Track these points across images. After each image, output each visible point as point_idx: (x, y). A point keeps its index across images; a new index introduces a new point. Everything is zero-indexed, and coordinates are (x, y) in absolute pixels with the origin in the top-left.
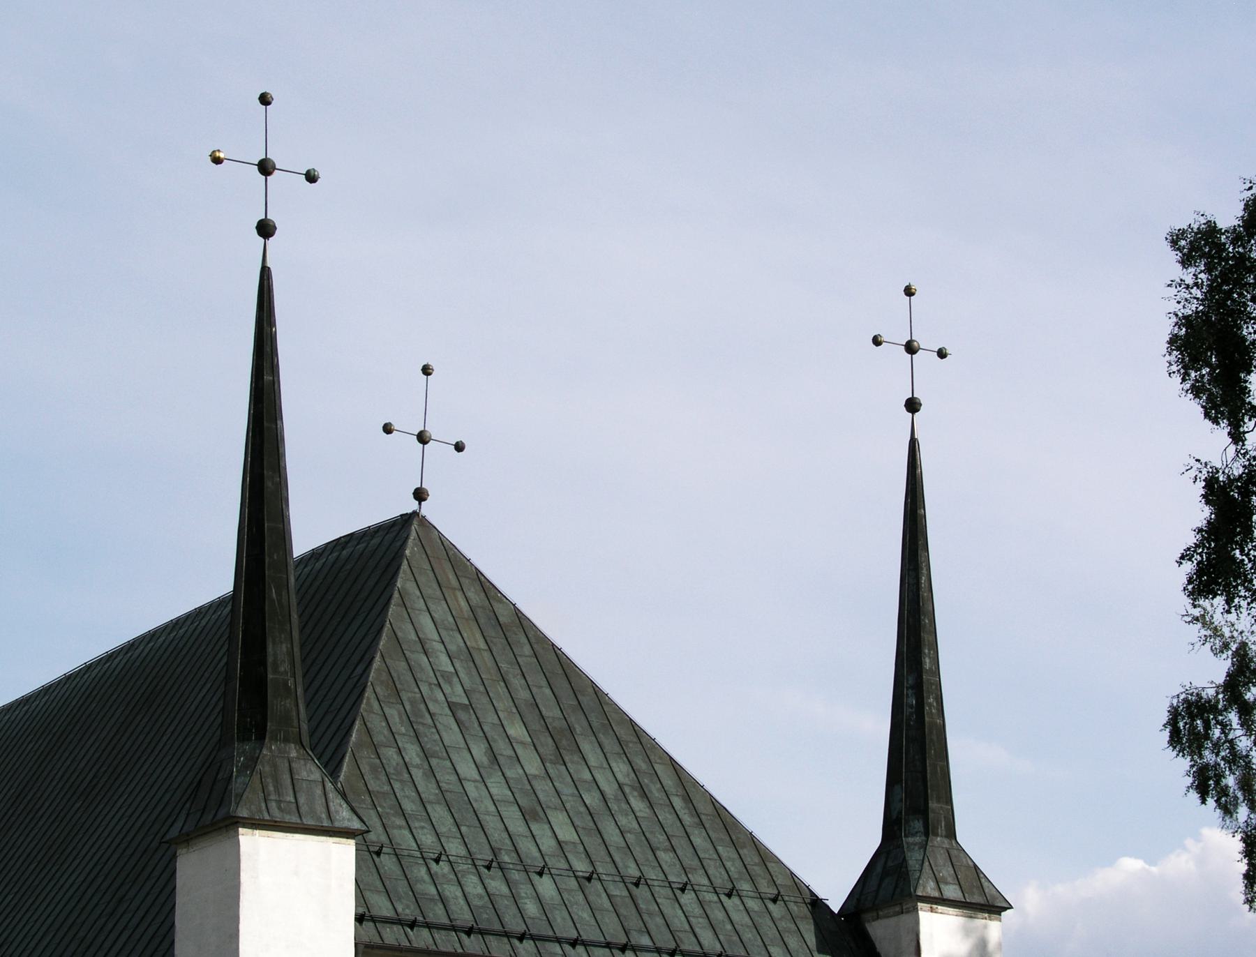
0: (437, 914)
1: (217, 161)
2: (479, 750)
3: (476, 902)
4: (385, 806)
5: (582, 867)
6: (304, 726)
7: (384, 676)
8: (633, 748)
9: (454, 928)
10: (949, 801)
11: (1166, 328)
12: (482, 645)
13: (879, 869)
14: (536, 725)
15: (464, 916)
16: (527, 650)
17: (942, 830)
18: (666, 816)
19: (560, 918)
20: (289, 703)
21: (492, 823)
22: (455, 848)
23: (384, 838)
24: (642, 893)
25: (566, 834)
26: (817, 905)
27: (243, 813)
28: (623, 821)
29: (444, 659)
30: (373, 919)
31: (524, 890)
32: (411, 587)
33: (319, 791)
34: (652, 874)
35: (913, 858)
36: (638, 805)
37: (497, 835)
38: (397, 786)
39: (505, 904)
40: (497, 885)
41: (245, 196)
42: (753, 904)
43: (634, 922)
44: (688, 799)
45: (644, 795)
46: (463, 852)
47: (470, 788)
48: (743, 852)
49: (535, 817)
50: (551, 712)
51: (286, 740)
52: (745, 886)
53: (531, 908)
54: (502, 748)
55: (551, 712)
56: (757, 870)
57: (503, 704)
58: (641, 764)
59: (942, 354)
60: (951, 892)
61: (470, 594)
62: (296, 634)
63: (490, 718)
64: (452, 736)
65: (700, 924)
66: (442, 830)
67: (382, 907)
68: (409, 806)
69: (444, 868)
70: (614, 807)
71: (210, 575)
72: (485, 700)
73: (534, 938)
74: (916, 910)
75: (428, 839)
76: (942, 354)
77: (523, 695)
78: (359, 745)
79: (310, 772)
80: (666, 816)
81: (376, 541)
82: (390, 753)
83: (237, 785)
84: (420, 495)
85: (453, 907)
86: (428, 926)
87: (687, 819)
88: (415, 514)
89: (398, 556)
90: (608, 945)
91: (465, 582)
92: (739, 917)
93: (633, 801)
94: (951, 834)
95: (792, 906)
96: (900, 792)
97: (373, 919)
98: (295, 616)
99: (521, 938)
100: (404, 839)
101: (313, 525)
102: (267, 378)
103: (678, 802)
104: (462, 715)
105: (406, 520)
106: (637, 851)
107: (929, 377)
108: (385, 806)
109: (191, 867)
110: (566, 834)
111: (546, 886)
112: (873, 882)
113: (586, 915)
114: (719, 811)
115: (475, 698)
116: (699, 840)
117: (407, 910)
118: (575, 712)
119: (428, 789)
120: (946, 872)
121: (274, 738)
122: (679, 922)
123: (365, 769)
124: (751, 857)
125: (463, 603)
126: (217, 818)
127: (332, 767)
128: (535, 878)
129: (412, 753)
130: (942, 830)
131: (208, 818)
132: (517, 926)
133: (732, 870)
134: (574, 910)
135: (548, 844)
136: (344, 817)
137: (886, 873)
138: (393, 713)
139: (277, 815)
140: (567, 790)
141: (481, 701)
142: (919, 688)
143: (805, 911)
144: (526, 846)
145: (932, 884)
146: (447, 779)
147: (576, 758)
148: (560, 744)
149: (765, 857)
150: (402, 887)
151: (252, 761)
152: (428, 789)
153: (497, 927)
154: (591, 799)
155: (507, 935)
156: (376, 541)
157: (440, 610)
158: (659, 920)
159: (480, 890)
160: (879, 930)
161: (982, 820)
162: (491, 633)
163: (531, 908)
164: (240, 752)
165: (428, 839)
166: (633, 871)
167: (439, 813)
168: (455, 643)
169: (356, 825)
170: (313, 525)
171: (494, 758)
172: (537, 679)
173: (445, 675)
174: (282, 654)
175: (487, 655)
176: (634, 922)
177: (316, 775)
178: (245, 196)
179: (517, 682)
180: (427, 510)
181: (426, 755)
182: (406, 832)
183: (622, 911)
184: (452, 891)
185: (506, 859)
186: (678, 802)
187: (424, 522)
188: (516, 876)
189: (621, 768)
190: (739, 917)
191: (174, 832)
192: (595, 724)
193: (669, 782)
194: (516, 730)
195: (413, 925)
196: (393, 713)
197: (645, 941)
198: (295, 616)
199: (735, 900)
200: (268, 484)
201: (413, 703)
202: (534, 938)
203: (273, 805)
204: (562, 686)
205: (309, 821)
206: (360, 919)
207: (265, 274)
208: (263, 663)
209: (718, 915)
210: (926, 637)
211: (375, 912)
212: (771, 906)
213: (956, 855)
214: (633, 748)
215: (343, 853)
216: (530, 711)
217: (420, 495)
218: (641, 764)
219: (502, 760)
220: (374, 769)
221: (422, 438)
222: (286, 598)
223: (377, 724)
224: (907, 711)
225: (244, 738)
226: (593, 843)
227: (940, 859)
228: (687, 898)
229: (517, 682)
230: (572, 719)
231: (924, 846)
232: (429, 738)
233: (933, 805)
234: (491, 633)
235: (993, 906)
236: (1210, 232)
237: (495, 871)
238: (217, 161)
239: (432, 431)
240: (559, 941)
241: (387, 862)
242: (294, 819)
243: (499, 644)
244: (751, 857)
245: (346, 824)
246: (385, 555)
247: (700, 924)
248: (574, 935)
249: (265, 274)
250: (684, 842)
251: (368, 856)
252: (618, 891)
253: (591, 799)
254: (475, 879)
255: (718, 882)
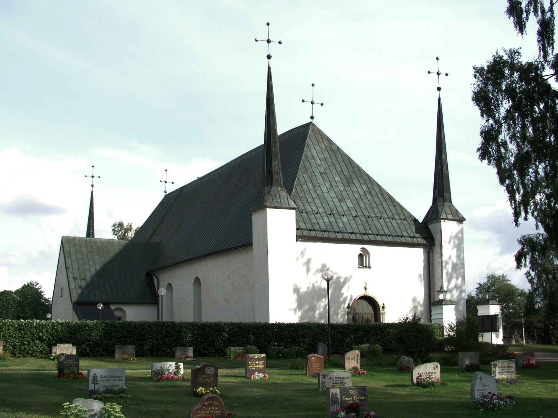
0: (317, 227)
1: (257, 41)
2: (328, 184)
3: (327, 224)
4: (304, 200)
5: (354, 213)
6: (282, 182)
7: (303, 166)
8: (368, 182)
9: (321, 231)
10: (450, 193)
11: (471, 95)
12: (329, 156)
13: (431, 211)
14: (342, 177)
15: (324, 228)
16: (340, 157)
17: (448, 200)
18: (376, 199)
19: (348, 227)
20: (278, 176)
21: (331, 203)
22: (321, 210)
23: (303, 208)
24: (370, 220)
25: (350, 205)
26: (416, 221)
27: (267, 205)
28: (365, 201)
29: (319, 161)
30: (301, 229)
31: (339, 220)
32: (310, 142)
33: (286, 198)
34: (372, 215)
35: (440, 208)
36: (369, 197)
37: (332, 206)
38: (306, 195)
39: (334, 224)
40: (332, 219)
41: (264, 48)
42: (399, 221)
43: (367, 227)
44: (382, 194)
45: (371, 194)
46: (323, 211)
47: (325, 194)
48: (397, 208)
49: (342, 201)
50: (346, 173)
51: (278, 186)
52: (397, 217)
53: (341, 225)
54: (334, 183)
55: (346, 173)
56: (400, 212)
57: (334, 172)
58: (370, 186)
59: (447, 75)
60: (450, 216)
61: (325, 143)
62: (279, 159)
63: (331, 176)
64: (321, 181)
65: (385, 227)
66: (318, 206)
67: (303, 226)
68: (310, 200)
69: (318, 215)
70: (363, 197)
71: (259, 140)
72: (329, 171)
73: (341, 232)
74: (440, 221)
75: (314, 208)
76: (447, 75)
77: (339, 169)
78: (297, 184)
79: (284, 193)
80: (376, 199)
81: (301, 130)
82: (305, 186)
83: (266, 198)
84: (312, 118)
85: (321, 225)
86: (315, 230)
87: (382, 200)
88: (311, 122)
89: (307, 134)
90: (360, 234)
91: (324, 140)
92: (395, 225)
93: (367, 196)
94: (450, 201)
95: (409, 222)
96: (437, 191)
97: (301, 229)
98: (279, 155)
99: (338, 233)
100: (308, 208)
101: (283, 127)
102: (270, 95)
103: (379, 195)
104: (323, 175)
105: (308, 125)
106: (368, 209)
107: (444, 81)
108: (304, 200)
109: (256, 218)
110: (350, 205)
111: (345, 219)
112: (430, 216)
113: (355, 226)
114: (390, 197)
115: (326, 171)
116: (385, 205)
117: (309, 227)
118: (352, 172)
119: (315, 196)
120: (449, 212)
121: (275, 185)
122: (379, 227)
123: (299, 191)
124: (398, 209)
125: (324, 146)
126: (261, 205)
127: (289, 192)
128: (342, 217)
129: (310, 186)
130: (448, 200)
131: (259, 206)
132: (338, 230)
133: (393, 212)
134: (352, 225)
135: (345, 208)
136: (292, 204)
137: (433, 212)
138: (305, 176)
139: (276, 205)
140: (351, 194)
141: (328, 171)
142: (441, 164)
143: (413, 222)
144: (340, 209)
145: (445, 215)
146: (319, 192)
147: (353, 185)
148: (349, 181)
149: (402, 209)
150: (308, 221)
151: (269, 192)
152: (315, 196)
153: (332, 230)
154: (357, 196)
155: (335, 232)
156: (301, 130)
157: (317, 148)
158: (374, 227)
159: (328, 221)
160: (432, 227)
161: (459, 198)
162: (331, 153)
163: (341, 225)
164: (266, 189)
165: (314, 208)
166: (367, 214)
167: (317, 201)
168: (321, 156)
169: (295, 206)
170: (283, 127)
171: (332, 186)
172: (343, 165)
173: (319, 165)
174: (276, 164)
175: (330, 159)
176: (367, 227)
177: (285, 194)
178: (264, 48)
179: (337, 166)
180: (314, 121)
181: (314, 186)
182: (309, 207)
183: (364, 225)
184: (321, 221)
185: (335, 212)
186: (379, 195)
187: (313, 125)
188: (337, 217)
189: (365, 187)
190: (395, 225)
191: (251, 209)
192: (358, 176)
193: (377, 190)
194: (337, 179)
195: (311, 230)
196: (305, 176)
197: (370, 232)
198: (279, 155)
199: (394, 220)
200: (271, 121)
201: (310, 173)
202: (341, 232)
203: (275, 202)
204: (349, 166)
205: (284, 206)
206: (297, 229)
207: (269, 68)
208: (272, 167)
209: (389, 224)
210: (443, 150)
211: (301, 227)
212: (403, 221)
213: (452, 207)
214: (368, 182)
215: (292, 213)
216: (341, 174)
217: (312, 118)
218: (370, 186)
219: (334, 187)
220: (301, 191)
221: (312, 103)
222: (277, 149)
223: (301, 179)
224: (438, 170)
225: (267, 186)
226: (357, 207)
227: (447, 208)
228: (382, 221)
229: (337, 166)
230: (352, 175)
231: (443, 205)
232: (315, 182)
233: (445, 194)
234: (331, 153)
235: (461, 220)
236: (482, 69)
237: (332, 216)
238: (257, 41)
239: (315, 101)
240: (348, 233)
241: (304, 214)
242: (280, 206)
243: (333, 155)
244: (398, 209)
245: (293, 206)
246: (303, 134)
247: (385, 227)
248: (352, 231)
249: (269, 68)
250: (381, 206)
251: (299, 212)
252: (363, 219)
253: (357, 196)
254: (326, 218)
255: (389, 216)
